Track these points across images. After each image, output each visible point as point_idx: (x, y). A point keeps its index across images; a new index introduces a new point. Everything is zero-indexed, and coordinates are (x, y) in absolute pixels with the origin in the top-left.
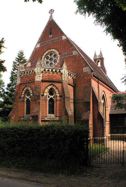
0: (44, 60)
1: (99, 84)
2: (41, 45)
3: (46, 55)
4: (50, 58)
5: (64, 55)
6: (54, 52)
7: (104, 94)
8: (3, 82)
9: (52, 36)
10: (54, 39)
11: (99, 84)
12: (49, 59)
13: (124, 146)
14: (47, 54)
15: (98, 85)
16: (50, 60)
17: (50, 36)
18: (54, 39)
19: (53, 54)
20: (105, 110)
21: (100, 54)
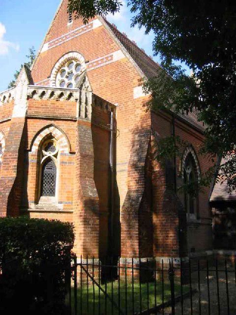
0: (55, 83)
1: (176, 128)
2: (50, 45)
3: (60, 68)
4: (69, 73)
5: (95, 64)
6: (76, 59)
7: (192, 152)
8: (83, 250)
9: (72, 22)
10: (76, 30)
11: (176, 128)
12: (66, 74)
13: (209, 293)
14: (63, 65)
15: (174, 128)
16: (67, 77)
17: (69, 24)
18: (76, 30)
19: (75, 63)
20: (42, 181)
21: (145, 71)
